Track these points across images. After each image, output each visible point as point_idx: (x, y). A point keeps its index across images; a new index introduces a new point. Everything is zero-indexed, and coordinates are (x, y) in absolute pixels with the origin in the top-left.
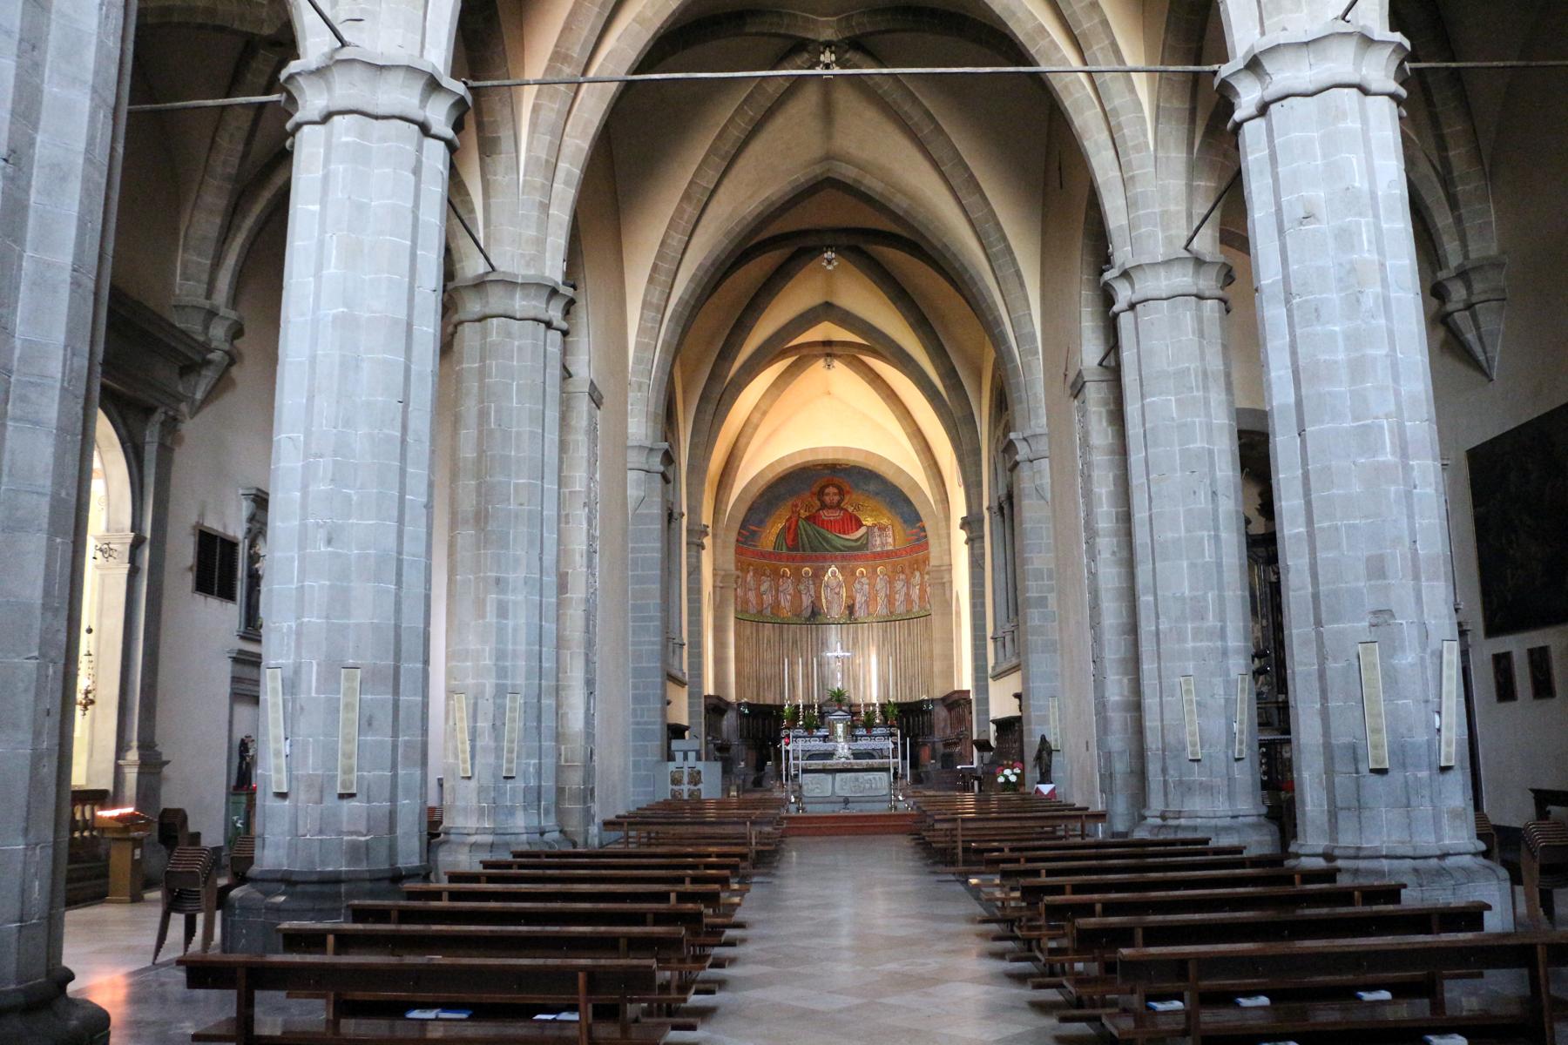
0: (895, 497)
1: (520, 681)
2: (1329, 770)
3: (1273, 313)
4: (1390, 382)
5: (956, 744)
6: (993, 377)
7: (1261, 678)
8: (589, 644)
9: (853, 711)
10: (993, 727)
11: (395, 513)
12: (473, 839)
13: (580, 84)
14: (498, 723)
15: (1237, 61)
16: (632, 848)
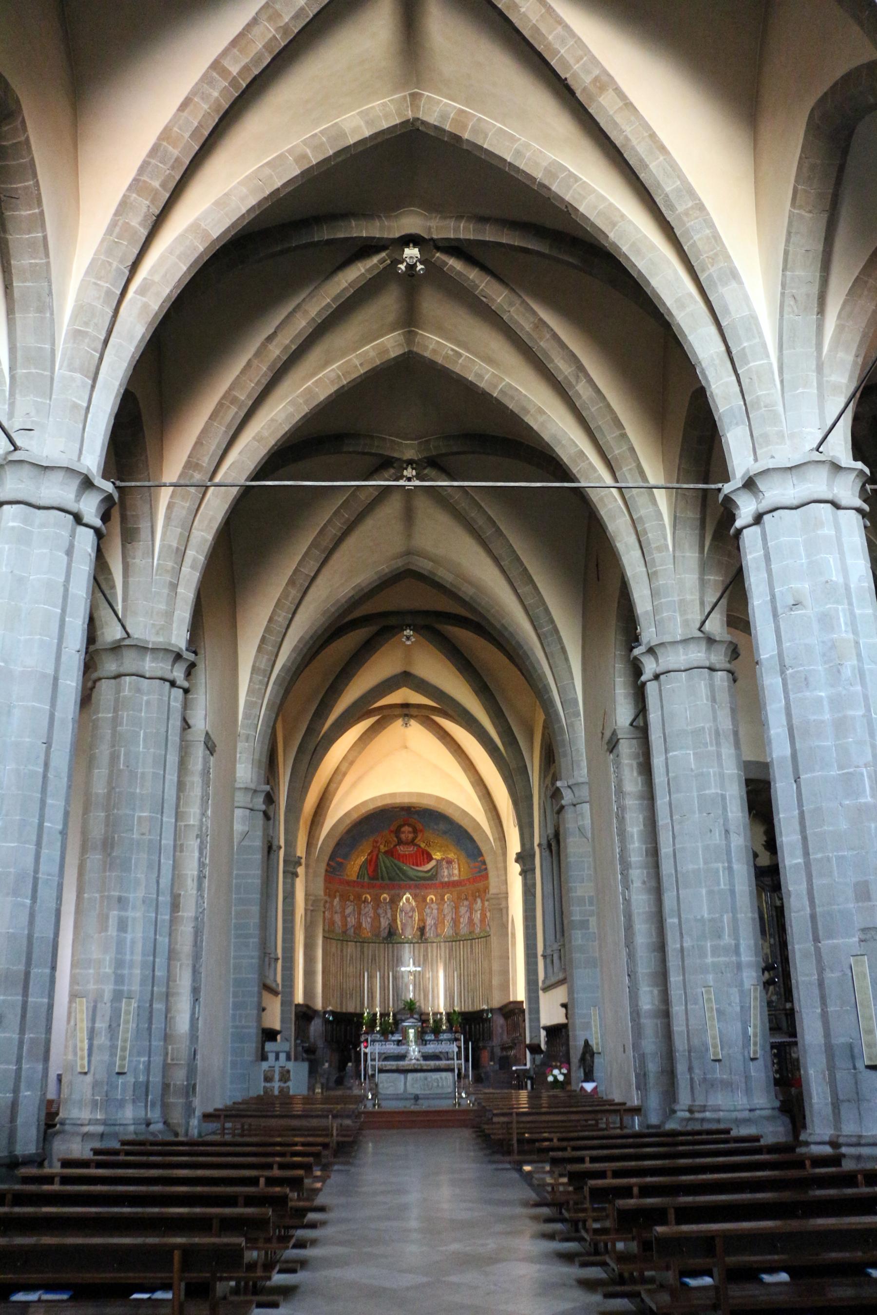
0: (458, 834)
1: (136, 987)
2: (831, 1068)
3: (771, 682)
4: (867, 738)
5: (511, 1048)
6: (543, 734)
7: (771, 988)
8: (196, 956)
9: (423, 1018)
10: (543, 1033)
11: (34, 838)
12: (86, 1129)
13: (207, 487)
14: (114, 1025)
15: (737, 481)
16: (228, 1138)
